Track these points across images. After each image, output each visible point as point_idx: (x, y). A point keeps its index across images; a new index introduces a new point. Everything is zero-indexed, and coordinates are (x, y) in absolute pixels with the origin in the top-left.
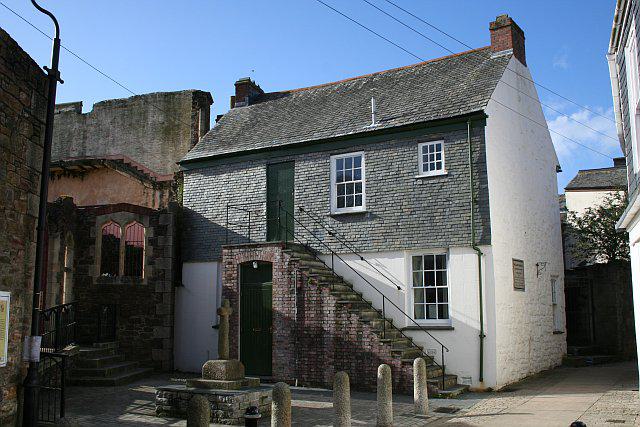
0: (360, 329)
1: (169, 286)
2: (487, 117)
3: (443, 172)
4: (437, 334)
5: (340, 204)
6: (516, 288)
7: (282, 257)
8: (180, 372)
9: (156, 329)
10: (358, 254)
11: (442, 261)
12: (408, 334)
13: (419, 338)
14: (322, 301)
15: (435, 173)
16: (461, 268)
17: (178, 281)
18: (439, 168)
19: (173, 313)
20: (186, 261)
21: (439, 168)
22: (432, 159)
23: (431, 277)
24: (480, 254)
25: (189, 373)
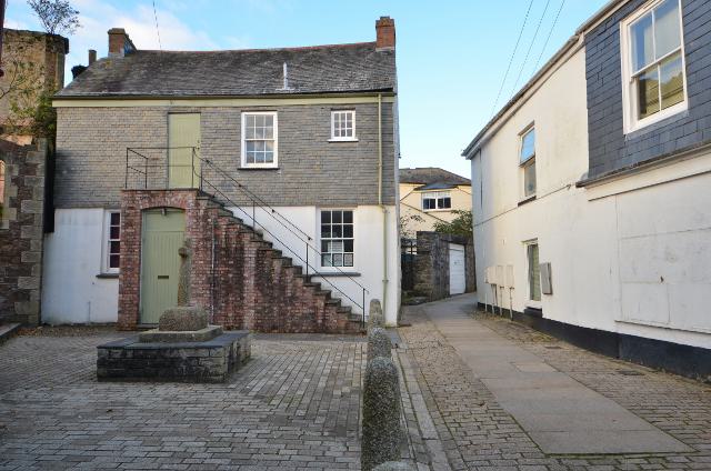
0: (282, 274)
1: (39, 230)
2: (381, 18)
3: (353, 138)
4: (330, 279)
5: (250, 160)
6: (465, 154)
7: (197, 205)
8: (46, 325)
9: (20, 278)
10: (257, 202)
11: (349, 217)
12: (315, 280)
13: (325, 284)
14: (242, 249)
15: (346, 138)
16: (366, 221)
17: (49, 227)
18: (350, 135)
19: (42, 263)
20: (61, 207)
21: (350, 134)
22: (343, 125)
23: (337, 228)
24: (386, 212)
25: (66, 325)
